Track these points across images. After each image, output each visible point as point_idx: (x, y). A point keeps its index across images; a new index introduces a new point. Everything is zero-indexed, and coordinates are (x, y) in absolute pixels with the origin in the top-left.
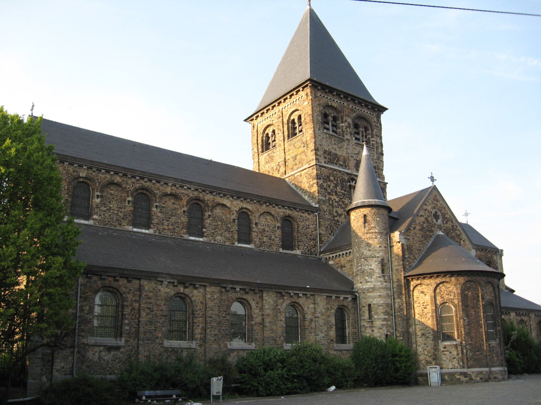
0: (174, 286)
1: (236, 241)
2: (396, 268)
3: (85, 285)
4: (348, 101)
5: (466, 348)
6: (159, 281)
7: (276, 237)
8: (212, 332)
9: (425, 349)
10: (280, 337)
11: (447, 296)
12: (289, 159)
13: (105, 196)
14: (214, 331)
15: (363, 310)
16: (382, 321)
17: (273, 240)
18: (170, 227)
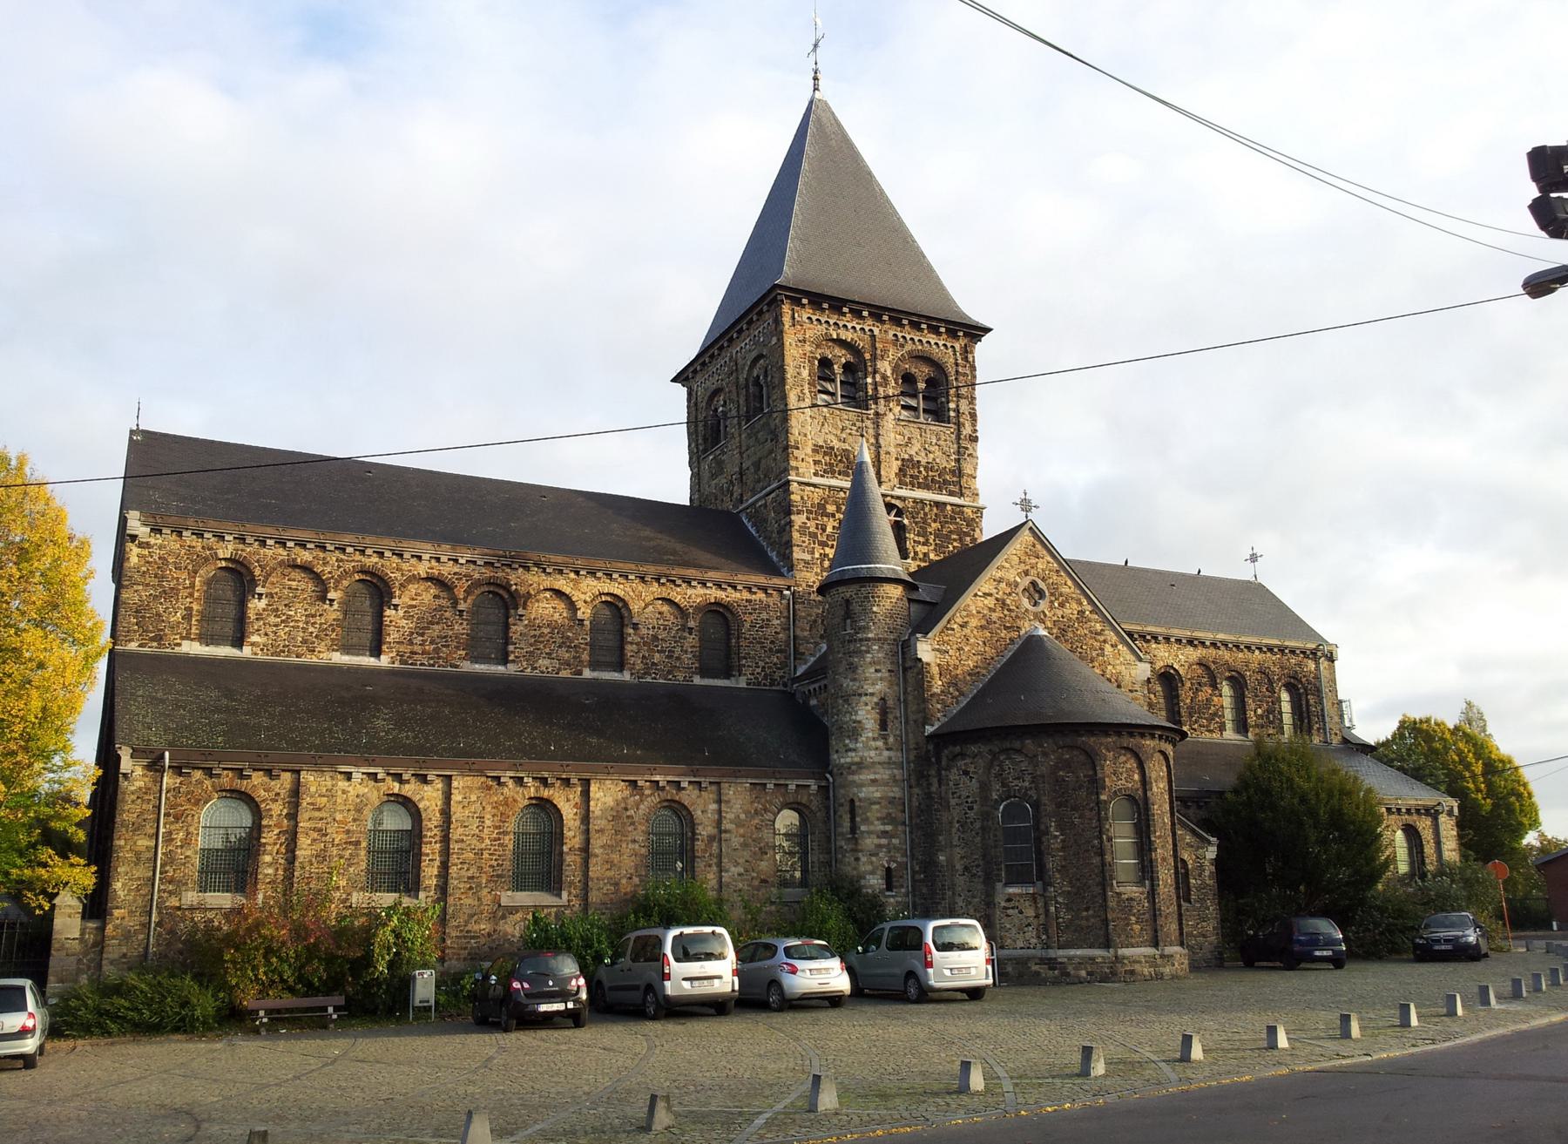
0: (376, 780)
1: (585, 667)
2: (914, 717)
3: (177, 790)
4: (883, 322)
5: (1057, 902)
6: (340, 773)
7: (686, 652)
8: (463, 873)
9: (970, 903)
10: (630, 878)
11: (1016, 782)
12: (748, 469)
13: (276, 593)
14: (468, 870)
15: (839, 813)
16: (878, 837)
17: (678, 658)
18: (427, 648)
